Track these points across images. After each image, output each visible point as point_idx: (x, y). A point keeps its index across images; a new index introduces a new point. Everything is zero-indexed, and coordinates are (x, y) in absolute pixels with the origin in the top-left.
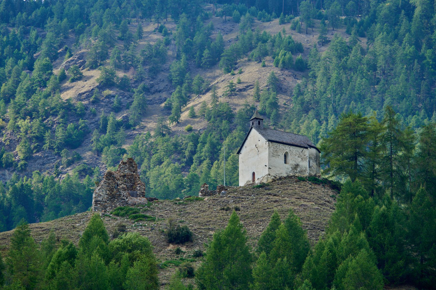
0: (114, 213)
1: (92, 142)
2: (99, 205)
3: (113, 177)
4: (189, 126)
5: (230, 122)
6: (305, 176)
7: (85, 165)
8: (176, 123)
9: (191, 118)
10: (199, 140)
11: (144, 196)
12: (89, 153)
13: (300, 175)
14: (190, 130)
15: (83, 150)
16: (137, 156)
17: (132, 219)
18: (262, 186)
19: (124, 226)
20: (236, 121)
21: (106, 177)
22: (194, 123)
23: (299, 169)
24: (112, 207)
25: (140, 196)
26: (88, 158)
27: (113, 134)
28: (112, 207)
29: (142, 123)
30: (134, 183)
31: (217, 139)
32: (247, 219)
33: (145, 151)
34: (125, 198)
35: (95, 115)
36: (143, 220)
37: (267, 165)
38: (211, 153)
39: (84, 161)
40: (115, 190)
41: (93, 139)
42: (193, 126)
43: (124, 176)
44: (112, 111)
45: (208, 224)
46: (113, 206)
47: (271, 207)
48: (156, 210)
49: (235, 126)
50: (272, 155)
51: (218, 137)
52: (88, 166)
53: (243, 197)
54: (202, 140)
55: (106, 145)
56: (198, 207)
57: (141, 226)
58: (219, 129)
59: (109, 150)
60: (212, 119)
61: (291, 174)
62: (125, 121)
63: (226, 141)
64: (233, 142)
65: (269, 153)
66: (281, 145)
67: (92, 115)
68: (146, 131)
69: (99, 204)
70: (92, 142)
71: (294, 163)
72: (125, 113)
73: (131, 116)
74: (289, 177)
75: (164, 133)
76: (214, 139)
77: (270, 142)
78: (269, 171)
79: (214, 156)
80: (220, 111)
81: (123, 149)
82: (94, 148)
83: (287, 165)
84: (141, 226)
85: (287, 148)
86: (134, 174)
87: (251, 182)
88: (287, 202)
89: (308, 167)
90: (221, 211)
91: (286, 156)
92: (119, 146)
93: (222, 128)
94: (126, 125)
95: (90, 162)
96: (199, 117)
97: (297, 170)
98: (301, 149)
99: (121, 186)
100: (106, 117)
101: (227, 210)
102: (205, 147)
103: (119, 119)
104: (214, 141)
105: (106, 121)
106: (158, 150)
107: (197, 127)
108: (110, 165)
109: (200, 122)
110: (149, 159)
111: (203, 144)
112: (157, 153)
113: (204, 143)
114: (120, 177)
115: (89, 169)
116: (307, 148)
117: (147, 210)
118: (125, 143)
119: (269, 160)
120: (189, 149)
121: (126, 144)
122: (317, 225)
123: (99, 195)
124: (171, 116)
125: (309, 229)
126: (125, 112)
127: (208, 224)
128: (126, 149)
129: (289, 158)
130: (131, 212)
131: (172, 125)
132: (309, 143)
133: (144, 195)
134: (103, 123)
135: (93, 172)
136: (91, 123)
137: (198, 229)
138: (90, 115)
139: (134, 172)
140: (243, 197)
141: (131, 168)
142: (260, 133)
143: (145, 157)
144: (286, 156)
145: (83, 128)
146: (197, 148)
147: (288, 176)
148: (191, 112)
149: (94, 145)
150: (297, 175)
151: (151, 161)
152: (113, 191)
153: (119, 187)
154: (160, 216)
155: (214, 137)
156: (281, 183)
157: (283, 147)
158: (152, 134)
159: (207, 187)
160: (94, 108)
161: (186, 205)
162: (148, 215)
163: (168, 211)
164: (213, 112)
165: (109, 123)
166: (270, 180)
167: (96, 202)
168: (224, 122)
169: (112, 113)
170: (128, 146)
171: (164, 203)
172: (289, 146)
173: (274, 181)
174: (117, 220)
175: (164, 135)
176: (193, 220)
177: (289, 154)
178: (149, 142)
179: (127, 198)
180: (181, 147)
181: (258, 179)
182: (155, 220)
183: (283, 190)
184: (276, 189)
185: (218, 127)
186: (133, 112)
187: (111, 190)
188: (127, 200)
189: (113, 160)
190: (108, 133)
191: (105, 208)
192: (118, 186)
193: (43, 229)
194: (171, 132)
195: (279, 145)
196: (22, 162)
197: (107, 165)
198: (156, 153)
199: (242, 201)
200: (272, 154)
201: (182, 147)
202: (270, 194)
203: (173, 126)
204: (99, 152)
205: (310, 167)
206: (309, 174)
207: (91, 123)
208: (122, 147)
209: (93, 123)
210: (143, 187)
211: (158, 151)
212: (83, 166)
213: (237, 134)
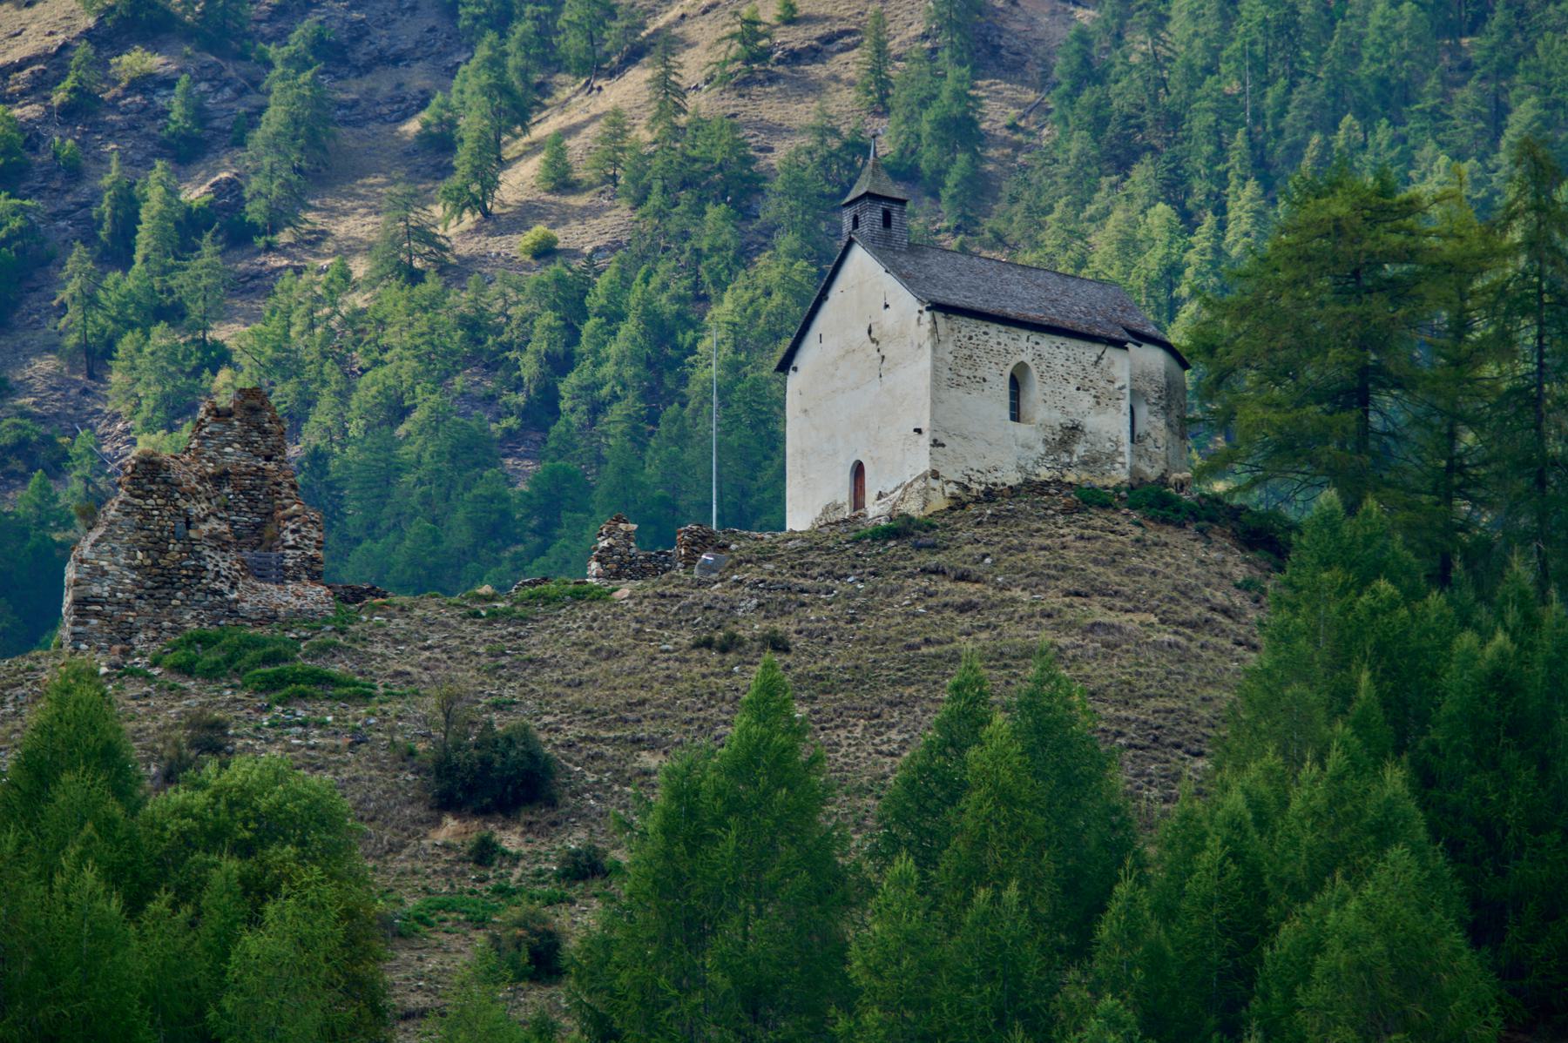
0: (169, 659)
1: (63, 307)
2: (94, 622)
3: (165, 482)
4: (539, 230)
5: (743, 212)
6: (1112, 484)
7: (27, 422)
8: (478, 215)
9: (550, 192)
10: (588, 300)
11: (315, 577)
12: (46, 365)
13: (1085, 476)
14: (545, 252)
15: (16, 350)
16: (285, 379)
17: (257, 691)
18: (901, 529)
19: (219, 726)
20: (771, 208)
21: (133, 481)
22: (564, 218)
23: (1080, 449)
24: (160, 630)
25: (296, 578)
26: (39, 386)
27: (166, 271)
28: (160, 630)
29: (310, 216)
30: (269, 514)
31: (678, 299)
32: (824, 692)
33: (325, 356)
34: (226, 588)
35: (74, 173)
36: (314, 697)
37: (925, 424)
38: (649, 364)
39: (20, 402)
40: (174, 547)
41: (63, 295)
42: (558, 233)
43: (220, 478)
44: (161, 156)
45: (631, 716)
46: (166, 624)
47: (941, 634)
48: (379, 648)
49: (769, 231)
50: (951, 377)
51: (681, 286)
52: (42, 429)
53: (808, 583)
54: (603, 301)
55: (131, 326)
56: (583, 634)
57: (303, 724)
58: (687, 246)
59: (147, 350)
60: (655, 200)
61: (1044, 474)
62: (225, 208)
63: (724, 309)
64: (757, 314)
65: (935, 370)
66: (994, 328)
67: (59, 176)
68: (326, 256)
69: (97, 614)
70: (63, 307)
71: (1057, 418)
72: (225, 168)
73: (255, 184)
74: (1032, 488)
75: (417, 264)
76: (664, 298)
77: (939, 316)
78: (932, 459)
79: (661, 383)
80: (695, 160)
81: (217, 345)
82: (71, 340)
83: (1021, 430)
84: (303, 724)
85: (1023, 344)
86: (271, 466)
87: (847, 512)
88: (1023, 610)
89: (1125, 437)
90: (695, 654)
91: (1016, 384)
92: (194, 327)
93: (705, 245)
94: (228, 223)
95: (51, 407)
96: (591, 186)
97: (1071, 453)
98: (1090, 352)
99: (205, 528)
100: (132, 185)
101: (724, 650)
102: (621, 334)
103: (195, 194)
104: (666, 305)
105: (129, 204)
106: (385, 349)
107: (579, 236)
108: (149, 427)
109: (596, 212)
110: (343, 396)
111: (609, 322)
112: (383, 363)
113: (613, 317)
114: (201, 480)
115: (48, 441)
116: (1120, 344)
117: (334, 645)
118: (226, 316)
119: (936, 401)
120: (540, 343)
121: (230, 319)
122: (1169, 724)
123: (94, 569)
124: (455, 181)
125: (1130, 746)
126: (226, 161)
127: (631, 716)
128: (231, 344)
129: (1035, 392)
130: (252, 654)
131: (456, 229)
132: (1135, 322)
133: (319, 574)
134: (114, 217)
135: (66, 457)
136: (54, 217)
137: (583, 739)
138: (49, 175)
139: (268, 459)
140: (808, 583)
141: (255, 436)
142: (893, 268)
143: (324, 383)
144: (1016, 384)
145: (17, 238)
146: (578, 343)
147: (1027, 482)
148: (551, 165)
149: (73, 327)
150: (1071, 477)
151: (354, 404)
152: (164, 552)
153: (192, 534)
154: (398, 674)
155: (661, 288)
156: (995, 519)
157: (1004, 338)
158: (360, 268)
159: (627, 535)
160: (69, 142)
161: (523, 620)
162: (336, 669)
163: (437, 653)
164: (657, 163)
165: (143, 215)
166: (939, 503)
167: (81, 603)
168: (714, 212)
169: (159, 164)
170: (238, 328)
171: (418, 612)
172: (1035, 337)
173: (957, 504)
174: (184, 693)
175: (415, 277)
176: (557, 695)
177: (1034, 373)
178: (344, 310)
179: (233, 586)
180: (500, 333)
181: (880, 496)
182: (369, 696)
183: (1005, 550)
184: (967, 548)
185: (685, 236)
186: (266, 161)
187: (157, 547)
188: (235, 595)
189: (165, 398)
190: (138, 266)
191: (125, 634)
192: (188, 524)
194: (453, 261)
195: (983, 326)
197: (136, 423)
198: (377, 363)
199: (803, 605)
200: (946, 374)
201: (504, 338)
202: (938, 571)
203: (463, 233)
204: (97, 356)
205: (1135, 438)
206: (1134, 471)
207: (54, 217)
208: (210, 334)
209: (65, 214)
210: (315, 534)
211: (387, 357)
212: (16, 426)
213: (774, 275)
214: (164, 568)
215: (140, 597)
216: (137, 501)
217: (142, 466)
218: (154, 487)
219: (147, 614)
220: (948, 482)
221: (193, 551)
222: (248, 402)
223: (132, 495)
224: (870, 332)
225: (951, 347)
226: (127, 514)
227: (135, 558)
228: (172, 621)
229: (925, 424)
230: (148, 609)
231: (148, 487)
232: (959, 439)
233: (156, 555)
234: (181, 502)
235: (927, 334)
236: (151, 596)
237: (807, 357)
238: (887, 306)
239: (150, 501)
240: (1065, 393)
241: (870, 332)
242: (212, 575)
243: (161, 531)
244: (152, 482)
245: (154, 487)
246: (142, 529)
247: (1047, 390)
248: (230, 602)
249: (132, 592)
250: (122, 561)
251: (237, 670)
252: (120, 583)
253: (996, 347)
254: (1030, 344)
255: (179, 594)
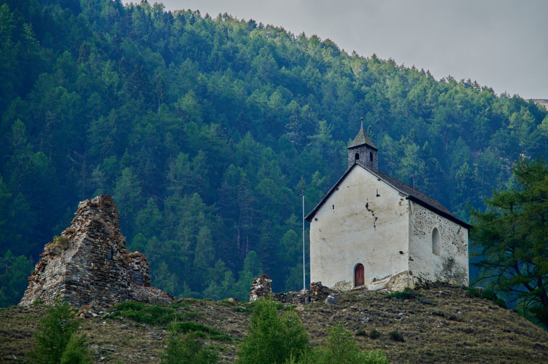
2: (74, 293)
3: (103, 232)
21: (90, 230)
24: (101, 300)
28: (101, 300)
37: (406, 249)
46: (104, 298)
50: (415, 231)
61: (443, 279)
66: (427, 211)
69: (75, 289)
74: (438, 284)
78: (410, 266)
97: (451, 271)
119: (410, 240)
147: (438, 282)
152: (103, 264)
159: (268, 284)
181: (375, 280)
187: (99, 261)
193: (135, 313)
196: (177, 107)
200: (413, 229)
214: (102, 272)
215: (92, 284)
216: (91, 239)
217: (94, 223)
218: (99, 234)
219: (95, 292)
220: (415, 277)
221: (114, 266)
222: (105, 201)
223: (89, 236)
224: (367, 206)
225: (415, 217)
226: (87, 245)
227: (90, 265)
228: (106, 297)
229: (406, 249)
230: (96, 290)
231: (96, 233)
232: (417, 258)
233: (99, 266)
234: (110, 242)
235: (406, 210)
236: (97, 284)
237: (325, 214)
238: (378, 196)
239: (97, 240)
240: (449, 244)
241: (367, 206)
242: (121, 278)
243: (101, 254)
244: (98, 231)
245: (99, 234)
246: (93, 252)
247: (444, 242)
248: (129, 291)
249: (89, 281)
250: (85, 266)
251: (158, 322)
252: (84, 276)
253: (428, 220)
254: (438, 221)
255: (108, 285)
